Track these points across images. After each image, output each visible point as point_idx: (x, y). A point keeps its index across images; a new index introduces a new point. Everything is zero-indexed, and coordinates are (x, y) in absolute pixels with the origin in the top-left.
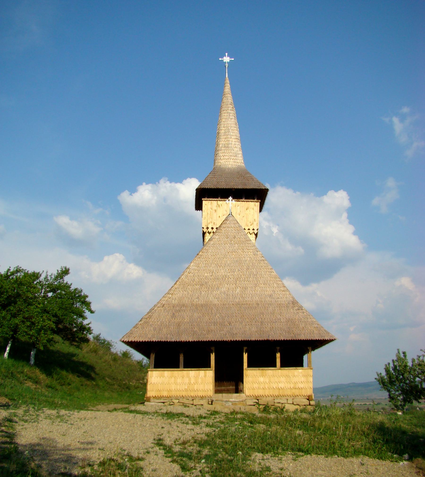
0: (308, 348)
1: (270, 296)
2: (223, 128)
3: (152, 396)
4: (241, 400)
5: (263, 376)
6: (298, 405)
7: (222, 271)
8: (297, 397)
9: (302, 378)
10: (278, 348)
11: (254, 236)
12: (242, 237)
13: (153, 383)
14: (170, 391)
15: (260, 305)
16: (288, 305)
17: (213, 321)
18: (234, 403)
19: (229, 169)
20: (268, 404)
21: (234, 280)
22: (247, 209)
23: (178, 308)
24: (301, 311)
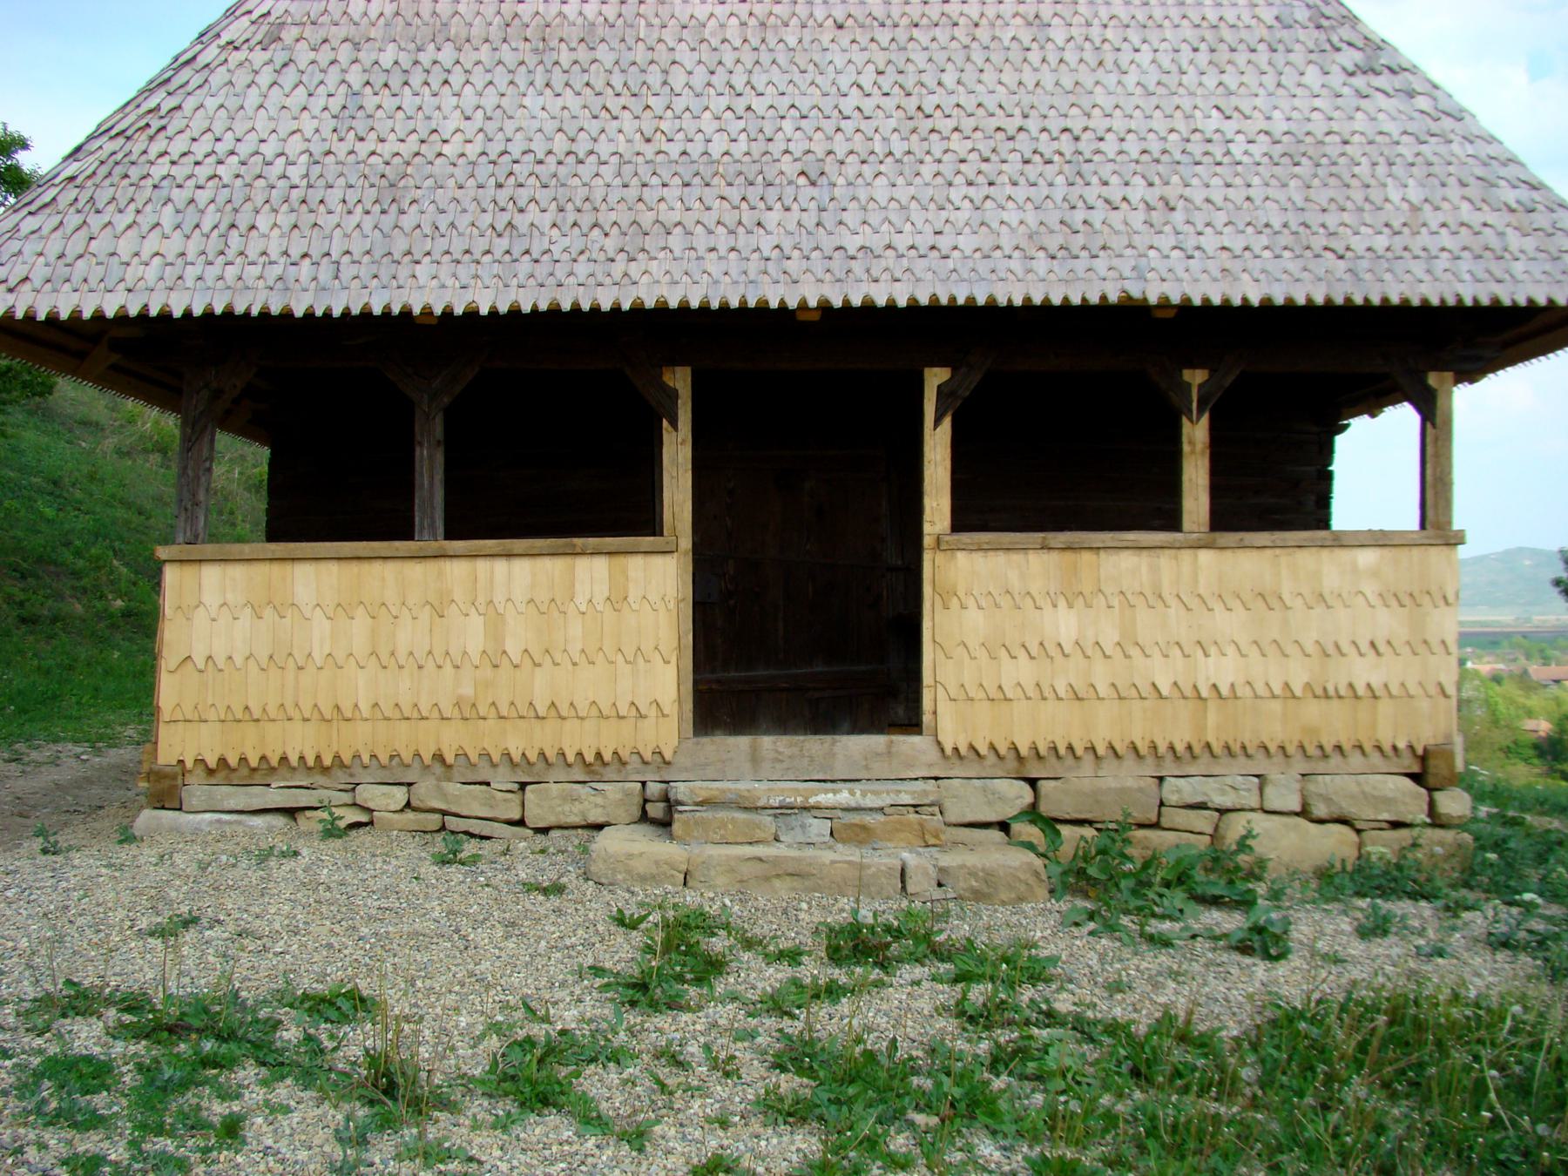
3: (200, 761)
5: (1071, 596)
8: (1336, 760)
9: (1383, 615)
10: (1196, 378)
13: (200, 661)
16: (1284, 34)
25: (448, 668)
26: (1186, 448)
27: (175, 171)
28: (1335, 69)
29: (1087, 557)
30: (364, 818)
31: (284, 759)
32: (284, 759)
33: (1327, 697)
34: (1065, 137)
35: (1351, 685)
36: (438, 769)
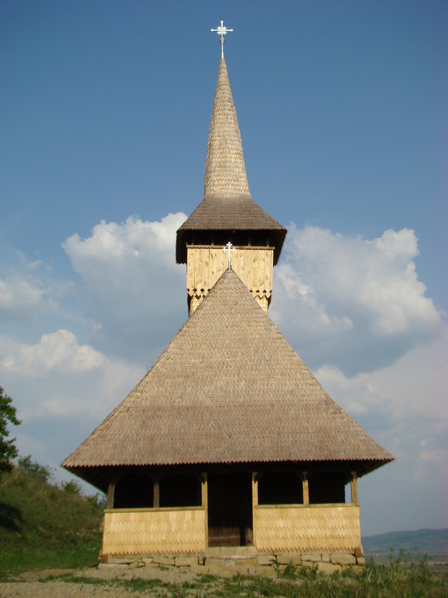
0: (352, 473)
1: (292, 392)
2: (217, 138)
3: (111, 554)
4: (249, 557)
5: (282, 517)
6: (339, 564)
7: (218, 355)
8: (337, 551)
10: (305, 473)
11: (265, 301)
12: (247, 302)
14: (139, 544)
15: (276, 407)
16: (319, 406)
17: (204, 432)
18: (239, 562)
19: (227, 199)
20: (291, 563)
21: (236, 369)
22: (254, 261)
23: (150, 413)
24: (338, 415)
25: (160, 533)
26: (304, 487)
27: (111, 437)
28: (329, 413)
29: (285, 509)
30: (143, 564)
31: (128, 553)
32: (128, 553)
33: (334, 538)
34: (277, 428)
35: (339, 535)
36: (158, 554)
